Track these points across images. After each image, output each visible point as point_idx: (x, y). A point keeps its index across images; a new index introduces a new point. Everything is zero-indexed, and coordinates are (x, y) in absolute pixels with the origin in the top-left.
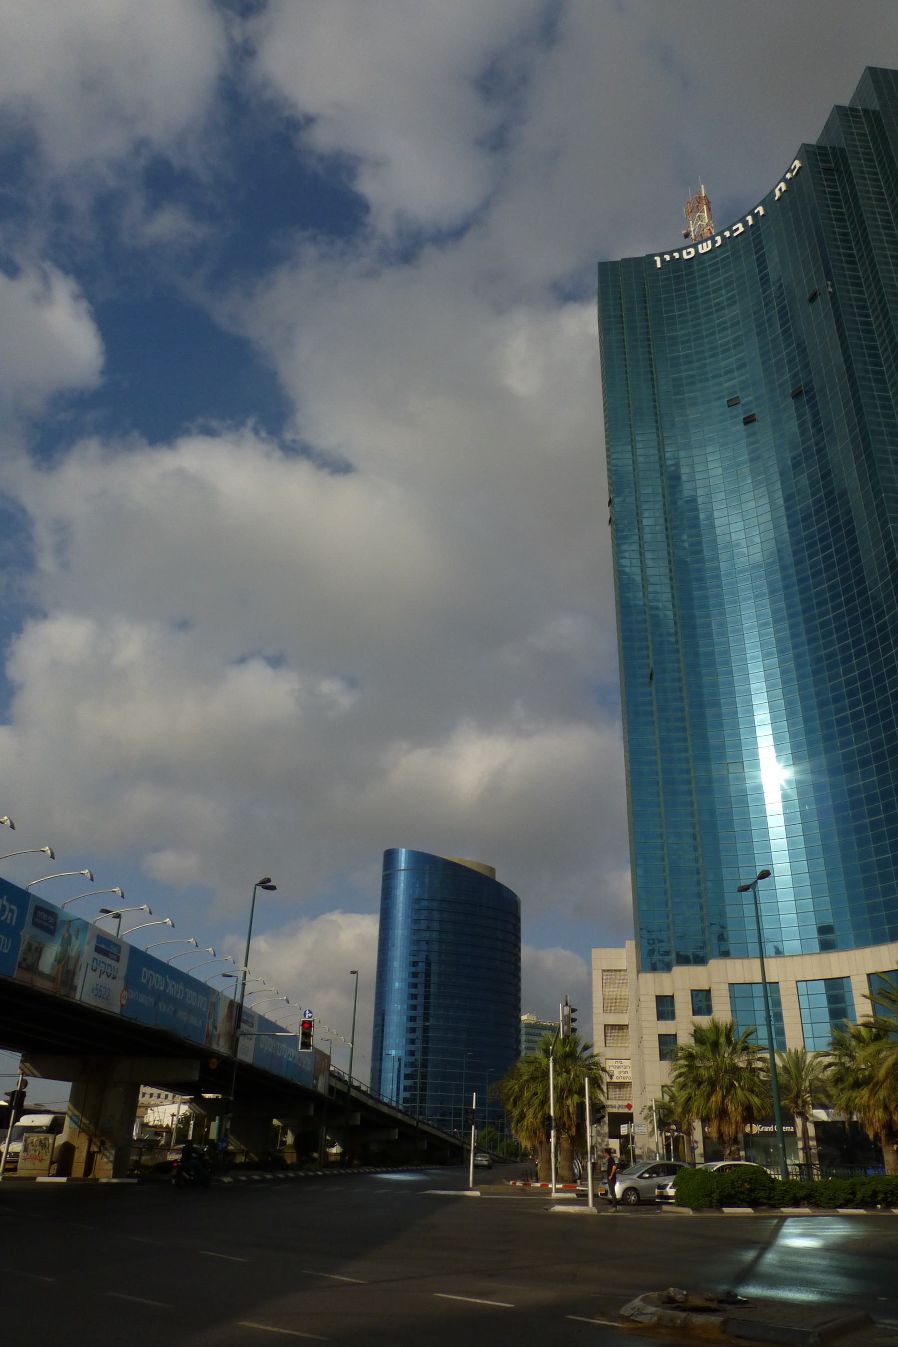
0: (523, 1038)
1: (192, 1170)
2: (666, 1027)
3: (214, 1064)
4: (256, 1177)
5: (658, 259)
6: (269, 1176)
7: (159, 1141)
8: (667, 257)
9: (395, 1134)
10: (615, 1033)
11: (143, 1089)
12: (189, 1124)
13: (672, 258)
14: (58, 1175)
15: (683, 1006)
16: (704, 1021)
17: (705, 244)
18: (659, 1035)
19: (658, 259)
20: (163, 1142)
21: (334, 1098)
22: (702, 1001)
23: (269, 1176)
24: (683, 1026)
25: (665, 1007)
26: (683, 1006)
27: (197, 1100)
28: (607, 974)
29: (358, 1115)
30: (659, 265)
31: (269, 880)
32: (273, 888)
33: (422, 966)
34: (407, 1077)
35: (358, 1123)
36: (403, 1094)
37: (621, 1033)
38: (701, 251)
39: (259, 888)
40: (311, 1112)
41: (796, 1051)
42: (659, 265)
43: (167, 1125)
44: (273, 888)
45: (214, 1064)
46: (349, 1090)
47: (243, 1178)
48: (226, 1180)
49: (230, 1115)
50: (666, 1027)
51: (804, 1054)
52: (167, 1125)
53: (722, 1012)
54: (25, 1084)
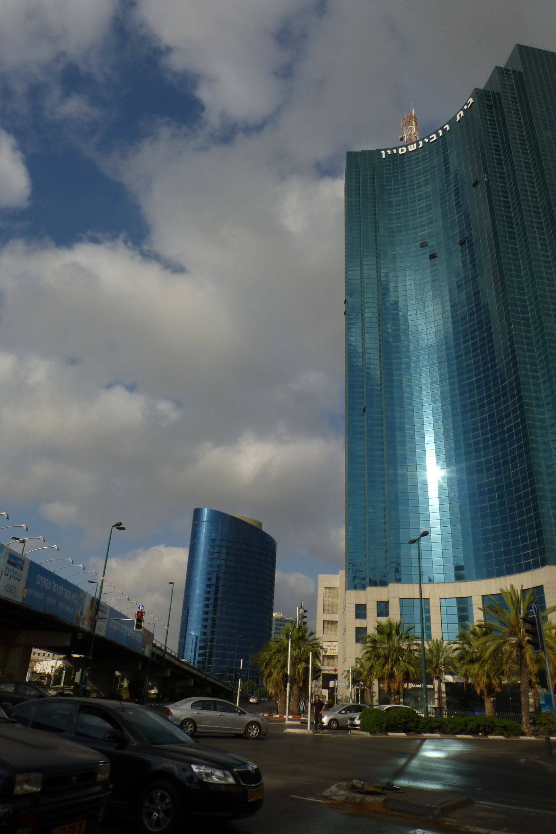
0: (274, 627)
2: (361, 623)
3: (80, 636)
5: (383, 152)
8: (389, 152)
9: (192, 683)
12: (62, 673)
15: (371, 611)
16: (384, 620)
17: (412, 145)
19: (383, 152)
22: (383, 608)
24: (371, 623)
25: (361, 611)
26: (371, 611)
27: (69, 658)
28: (327, 590)
29: (169, 671)
30: (384, 157)
31: (121, 524)
32: (123, 529)
34: (201, 648)
35: (169, 675)
37: (333, 626)
38: (410, 150)
39: (114, 529)
40: (140, 668)
41: (437, 640)
42: (384, 157)
43: (49, 673)
44: (123, 529)
45: (80, 636)
49: (89, 668)
50: (361, 623)
52: (49, 673)
53: (395, 616)
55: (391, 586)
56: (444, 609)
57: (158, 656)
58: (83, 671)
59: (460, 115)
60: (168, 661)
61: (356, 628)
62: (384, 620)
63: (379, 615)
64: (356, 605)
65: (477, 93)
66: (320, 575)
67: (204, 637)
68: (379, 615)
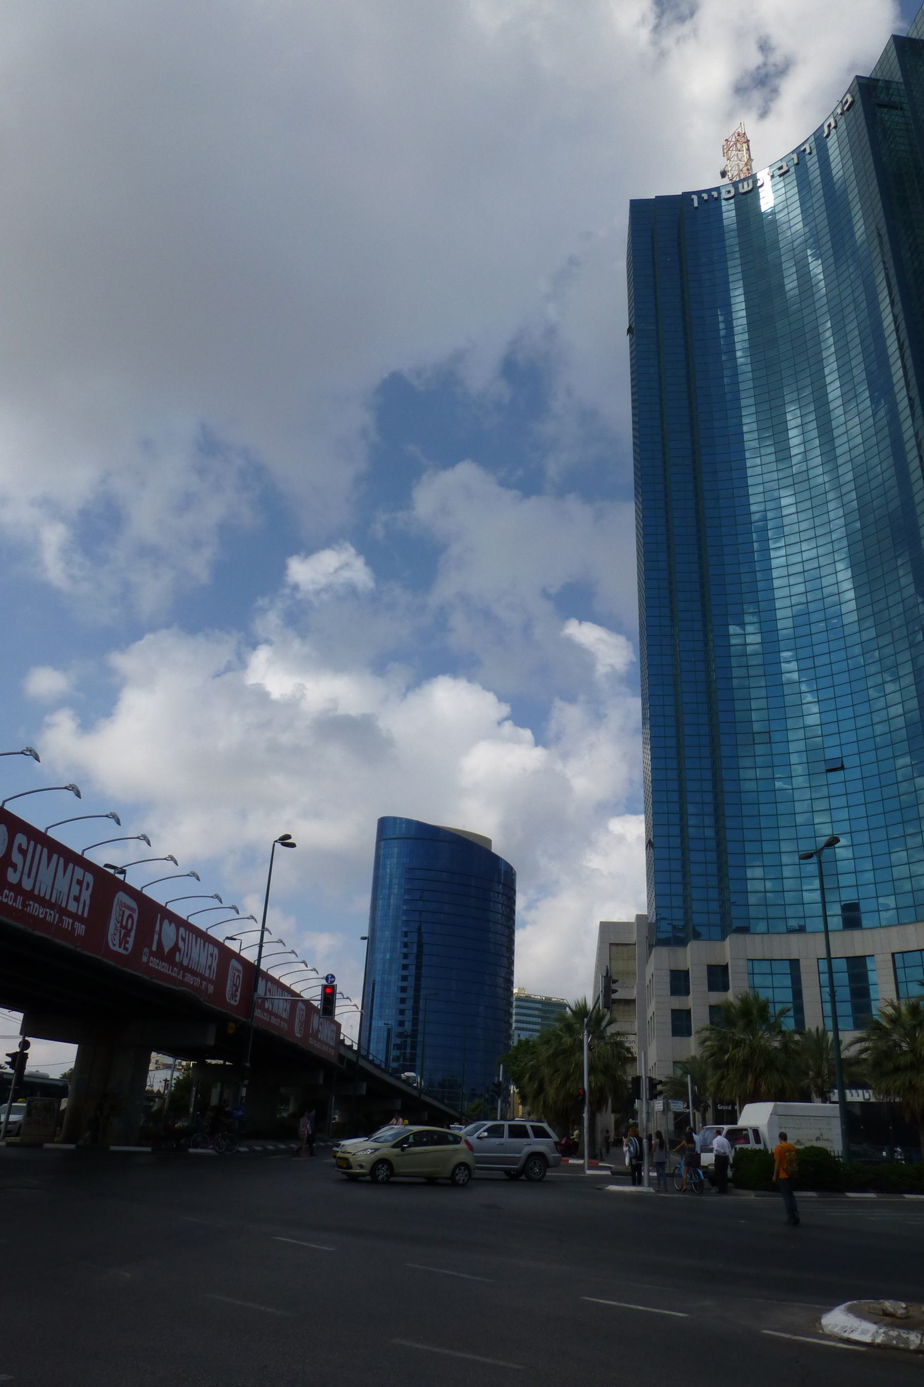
1: (171, 1131)
2: (678, 1003)
3: (231, 1028)
4: (271, 1147)
5: (695, 197)
6: (282, 1147)
7: (151, 1107)
8: (705, 196)
10: (621, 1008)
11: (154, 1056)
12: (190, 1092)
13: (710, 196)
14: (67, 1140)
15: (698, 981)
16: (716, 998)
17: (745, 183)
18: (672, 1010)
19: (695, 197)
20: (155, 1108)
21: (344, 1067)
22: (718, 976)
23: (282, 1147)
24: (699, 1001)
25: (679, 982)
26: (698, 981)
28: (614, 948)
29: (365, 1085)
30: (696, 204)
31: (288, 837)
32: (293, 845)
33: (414, 937)
34: (398, 1047)
35: (364, 1093)
36: (394, 1053)
37: (627, 1008)
38: (741, 191)
39: (278, 845)
40: (321, 1081)
41: (817, 1029)
42: (696, 204)
43: (159, 1091)
44: (293, 845)
45: (231, 1028)
46: (358, 1060)
47: (258, 1148)
48: (243, 1149)
49: (246, 1082)
50: (678, 1003)
51: (825, 1032)
52: (159, 1091)
54: (25, 1045)
55: (692, 946)
56: (900, 972)
57: (350, 1062)
58: (222, 1087)
59: (15, 867)
60: (362, 1069)
61: (672, 1010)
62: (716, 998)
63: (712, 987)
64: (672, 971)
65: (859, 84)
66: (20, 1016)
67: (400, 1029)
68: (712, 987)
